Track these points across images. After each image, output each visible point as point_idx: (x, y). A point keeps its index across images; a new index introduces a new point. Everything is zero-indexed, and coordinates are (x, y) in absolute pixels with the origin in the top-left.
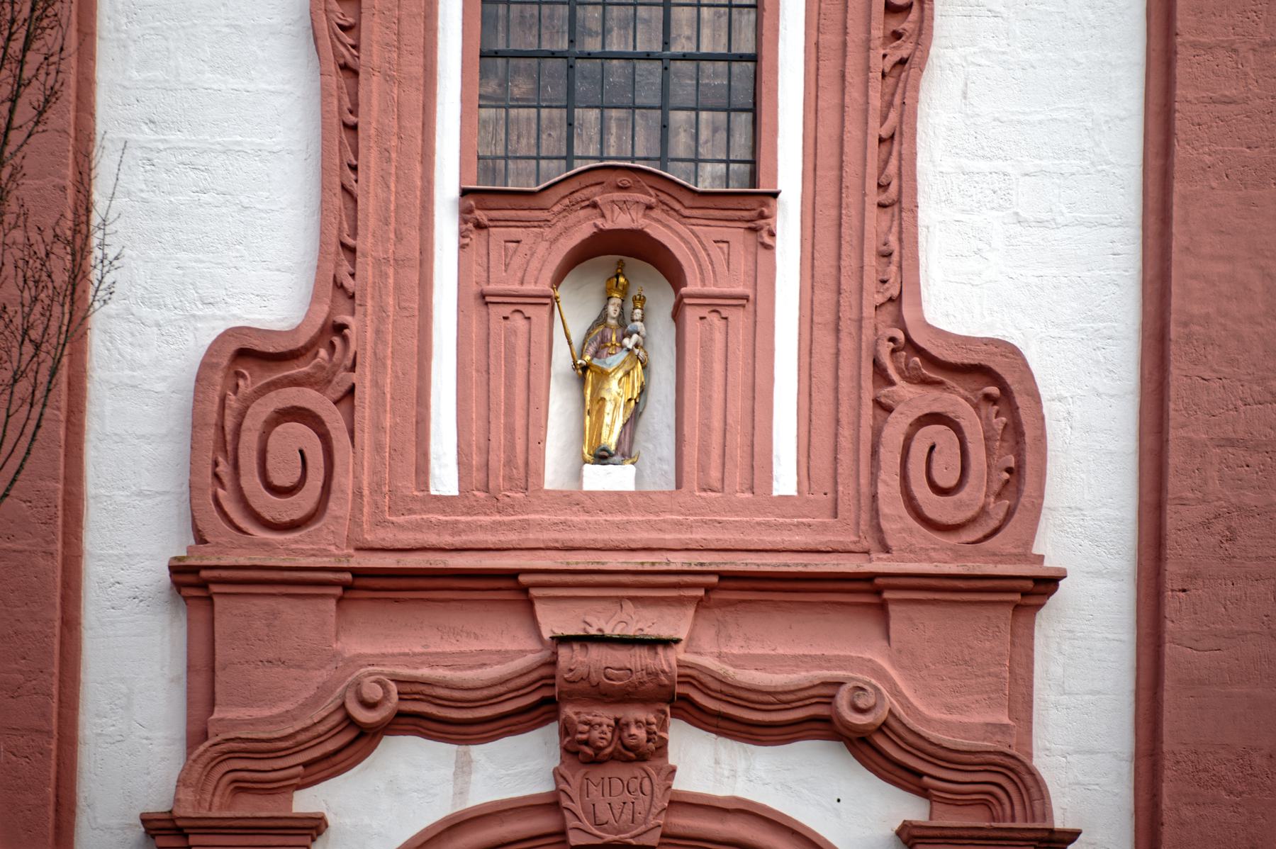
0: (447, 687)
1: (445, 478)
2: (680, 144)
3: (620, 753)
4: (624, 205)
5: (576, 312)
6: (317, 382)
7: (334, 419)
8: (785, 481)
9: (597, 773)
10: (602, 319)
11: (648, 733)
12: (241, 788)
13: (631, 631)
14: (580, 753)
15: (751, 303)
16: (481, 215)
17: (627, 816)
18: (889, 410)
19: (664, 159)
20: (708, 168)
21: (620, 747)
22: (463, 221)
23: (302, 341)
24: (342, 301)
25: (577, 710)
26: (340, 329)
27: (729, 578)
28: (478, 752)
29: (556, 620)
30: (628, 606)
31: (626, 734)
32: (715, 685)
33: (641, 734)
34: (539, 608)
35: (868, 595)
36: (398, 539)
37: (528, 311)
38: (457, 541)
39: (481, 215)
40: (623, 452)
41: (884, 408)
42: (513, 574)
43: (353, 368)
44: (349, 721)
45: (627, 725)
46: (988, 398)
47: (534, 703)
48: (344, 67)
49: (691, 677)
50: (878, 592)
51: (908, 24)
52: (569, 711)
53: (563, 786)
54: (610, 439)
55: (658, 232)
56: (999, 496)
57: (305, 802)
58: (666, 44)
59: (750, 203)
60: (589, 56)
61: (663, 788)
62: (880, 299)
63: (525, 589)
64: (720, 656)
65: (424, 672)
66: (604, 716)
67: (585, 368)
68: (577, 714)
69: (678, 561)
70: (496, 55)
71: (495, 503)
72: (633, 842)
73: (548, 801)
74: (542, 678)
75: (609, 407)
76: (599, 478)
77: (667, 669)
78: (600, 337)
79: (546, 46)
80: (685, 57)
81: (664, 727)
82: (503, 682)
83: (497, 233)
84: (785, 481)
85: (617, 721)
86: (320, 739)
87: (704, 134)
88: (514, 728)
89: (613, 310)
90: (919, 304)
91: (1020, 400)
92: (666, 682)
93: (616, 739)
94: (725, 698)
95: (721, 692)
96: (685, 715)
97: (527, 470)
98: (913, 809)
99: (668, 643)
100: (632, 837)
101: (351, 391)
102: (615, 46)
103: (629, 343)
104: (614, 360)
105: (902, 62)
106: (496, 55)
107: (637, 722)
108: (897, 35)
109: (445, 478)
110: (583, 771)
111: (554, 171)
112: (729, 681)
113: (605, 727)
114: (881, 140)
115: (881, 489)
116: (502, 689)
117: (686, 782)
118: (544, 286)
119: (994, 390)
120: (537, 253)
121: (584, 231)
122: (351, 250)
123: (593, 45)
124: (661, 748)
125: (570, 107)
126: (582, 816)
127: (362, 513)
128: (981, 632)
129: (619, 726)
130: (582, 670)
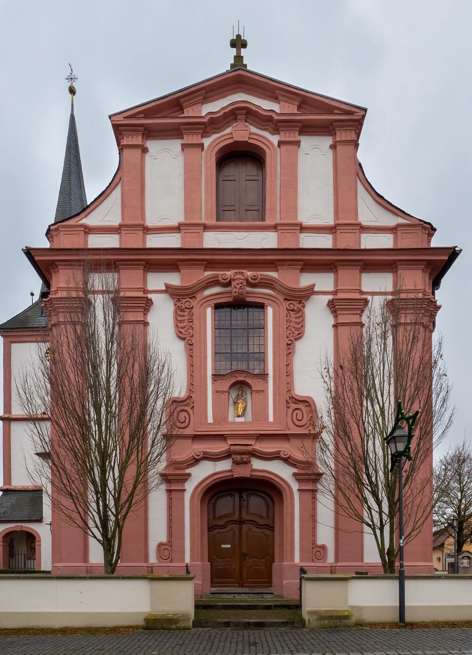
1: (210, 420)
2: (251, 367)
4: (241, 376)
5: (234, 394)
6: (187, 405)
7: (190, 411)
8: (271, 419)
9: (238, 466)
10: (238, 395)
12: (176, 469)
13: (244, 444)
14: (236, 463)
15: (264, 392)
16: (216, 379)
17: (244, 472)
18: (289, 408)
19: (248, 369)
20: (256, 370)
22: (212, 379)
23: (185, 399)
24: (191, 392)
26: (191, 397)
27: (261, 435)
28: (217, 463)
29: (230, 442)
30: (244, 440)
33: (246, 459)
34: (227, 440)
35: (286, 437)
36: (202, 430)
37: (224, 393)
38: (213, 430)
39: (216, 379)
40: (243, 415)
41: (288, 407)
42: (222, 435)
43: (193, 403)
44: (194, 458)
46: (307, 406)
47: (227, 455)
48: (191, 356)
49: (254, 450)
50: (288, 437)
51: (290, 347)
52: (233, 456)
54: (240, 413)
55: (247, 381)
56: (309, 421)
57: (187, 471)
58: (248, 351)
59: (264, 376)
60: (234, 353)
62: (287, 390)
63: (225, 437)
64: (260, 447)
65: (207, 450)
67: (235, 403)
69: (252, 432)
70: (218, 353)
71: (219, 423)
75: (239, 408)
76: (238, 420)
78: (238, 398)
79: (227, 352)
80: (251, 353)
81: (250, 458)
82: (221, 452)
83: (219, 382)
84: (271, 419)
86: (190, 461)
87: (255, 365)
89: (240, 393)
90: (294, 391)
91: (313, 406)
97: (225, 418)
98: (296, 471)
99: (250, 445)
101: (193, 407)
102: (239, 351)
103: (243, 398)
104: (239, 401)
105: (290, 353)
106: (218, 353)
108: (289, 349)
109: (210, 420)
111: (229, 371)
114: (287, 365)
115: (288, 420)
118: (227, 389)
119: (308, 404)
120: (225, 385)
121: (234, 381)
122: (193, 384)
123: (235, 352)
124: (250, 462)
125: (231, 361)
128: (307, 443)
129: (242, 458)
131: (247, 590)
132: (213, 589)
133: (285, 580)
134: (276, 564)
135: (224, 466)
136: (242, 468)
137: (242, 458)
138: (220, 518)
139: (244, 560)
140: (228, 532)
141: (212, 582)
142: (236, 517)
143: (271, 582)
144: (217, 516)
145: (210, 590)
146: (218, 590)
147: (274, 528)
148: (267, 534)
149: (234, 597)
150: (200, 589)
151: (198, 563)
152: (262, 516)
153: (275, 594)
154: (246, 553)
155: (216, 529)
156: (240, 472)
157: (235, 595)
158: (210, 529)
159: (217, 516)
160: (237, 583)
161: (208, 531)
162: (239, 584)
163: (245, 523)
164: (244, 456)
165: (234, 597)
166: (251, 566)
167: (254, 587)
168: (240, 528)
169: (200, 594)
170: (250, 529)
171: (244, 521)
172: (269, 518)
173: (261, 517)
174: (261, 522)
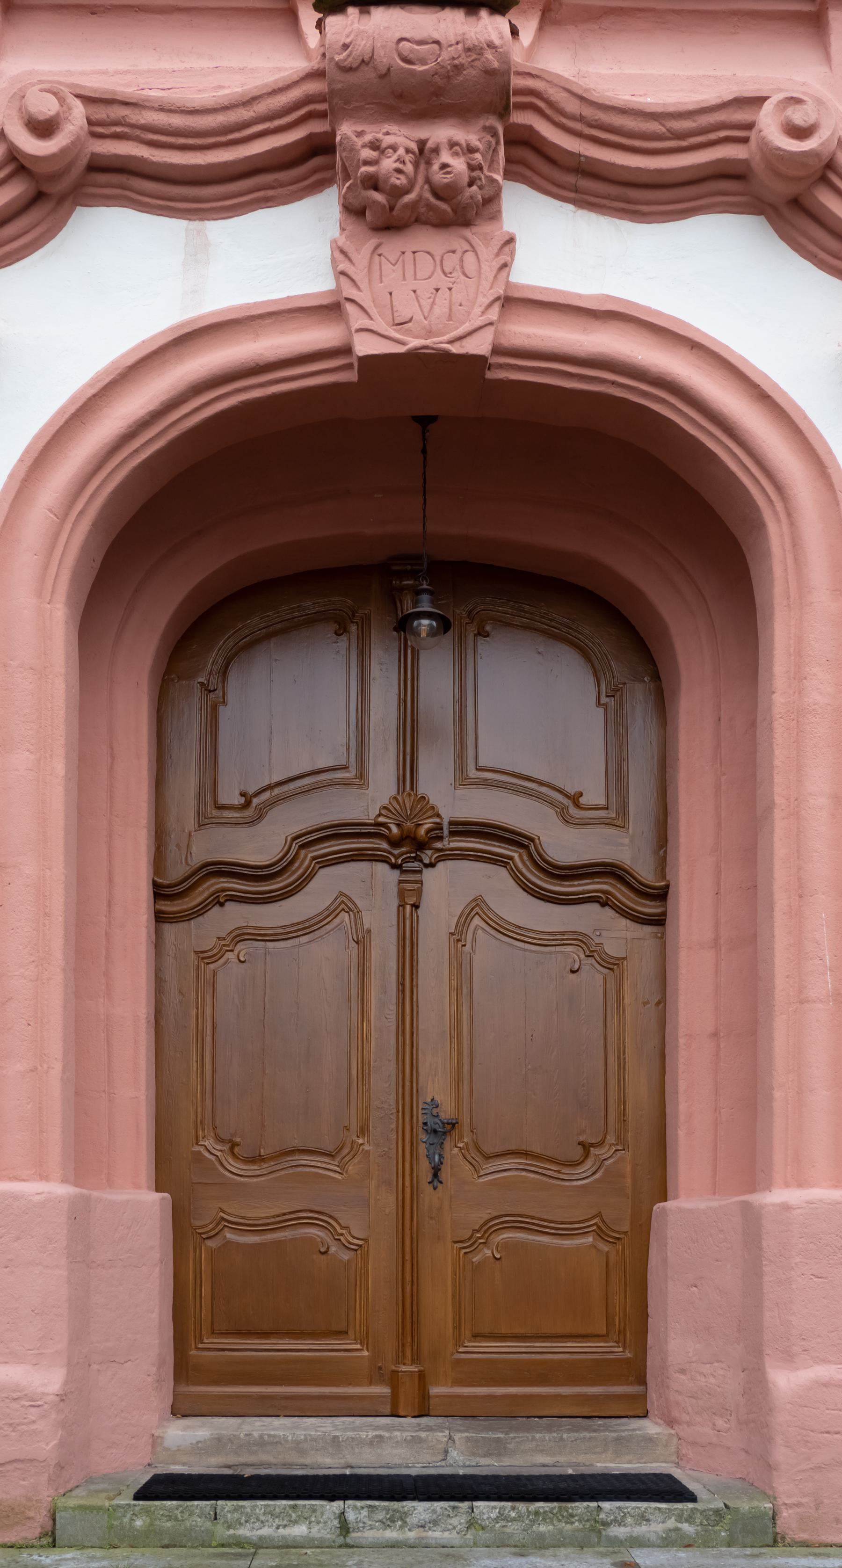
0: (161, 109)
3: (429, 206)
9: (393, 245)
11: (471, 168)
17: (441, 309)
21: (428, 195)
25: (359, 128)
28: (222, 232)
31: (436, 167)
32: (572, 106)
45: (436, 151)
53: (349, 291)
61: (496, 264)
66: (400, 136)
68: (360, 134)
72: (455, 349)
73: (325, 301)
74: (309, 100)
77: (497, 42)
85: (422, 144)
88: (270, 193)
92: (496, 65)
93: (420, 180)
94: (588, 131)
95: (581, 119)
96: (528, 173)
100: (451, 342)
107: (452, 144)
110: (373, 242)
112: (595, 97)
113: (401, 151)
116: (245, 114)
117: (533, 271)
124: (489, 206)
126: (373, 312)
127: (444, 1531)
129: (424, 153)
130: (362, 46)
131: (450, 1448)
132: (190, 1442)
133: (789, 1358)
134: (692, 1204)
135: (276, 259)
136: (425, 264)
137: (424, 153)
138: (252, 808)
139: (436, 1172)
140: (305, 928)
141: (184, 1368)
142: (371, 800)
143: (635, 1371)
144: (230, 795)
145: (155, 1441)
146: (218, 1443)
147: (662, 895)
148: (612, 949)
149: (345, 1528)
150: (46, 1447)
151: (32, 1188)
152: (576, 799)
153: (708, 1501)
154: (447, 1111)
155: (218, 900)
156: (406, 308)
157: (356, 1510)
158: (172, 898)
159: (230, 795)
160: (376, 1375)
161: (160, 918)
162: (394, 1380)
163: (446, 856)
164: (440, 133)
165: (345, 1528)
166: (488, 1229)
167: (514, 1413)
168: (402, 894)
169: (46, 1494)
170: (477, 906)
171: (436, 834)
172: (623, 809)
173: (569, 806)
174: (565, 845)
